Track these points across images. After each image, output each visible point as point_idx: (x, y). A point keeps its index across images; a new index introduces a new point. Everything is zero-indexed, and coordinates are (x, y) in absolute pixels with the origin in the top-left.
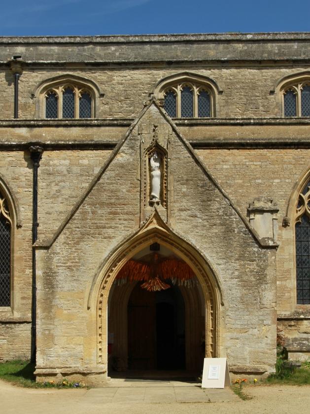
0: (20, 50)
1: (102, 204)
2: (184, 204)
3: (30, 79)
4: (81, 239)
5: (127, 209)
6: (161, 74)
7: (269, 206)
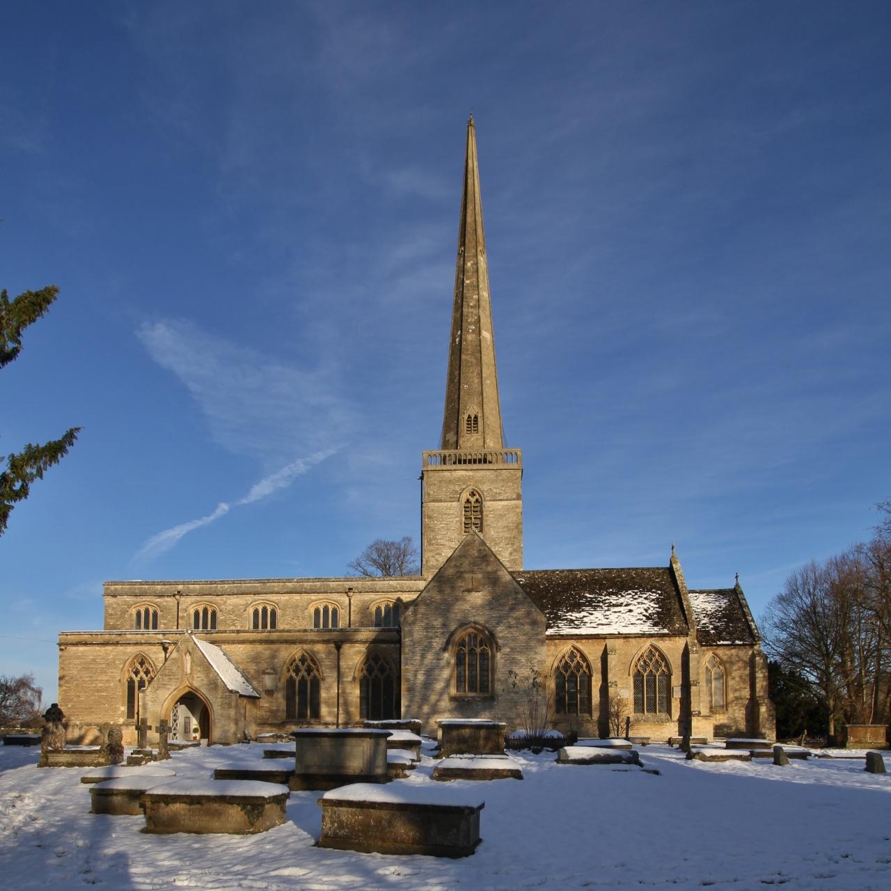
1: (166, 675)
2: (199, 675)
4: (157, 690)
5: (177, 677)
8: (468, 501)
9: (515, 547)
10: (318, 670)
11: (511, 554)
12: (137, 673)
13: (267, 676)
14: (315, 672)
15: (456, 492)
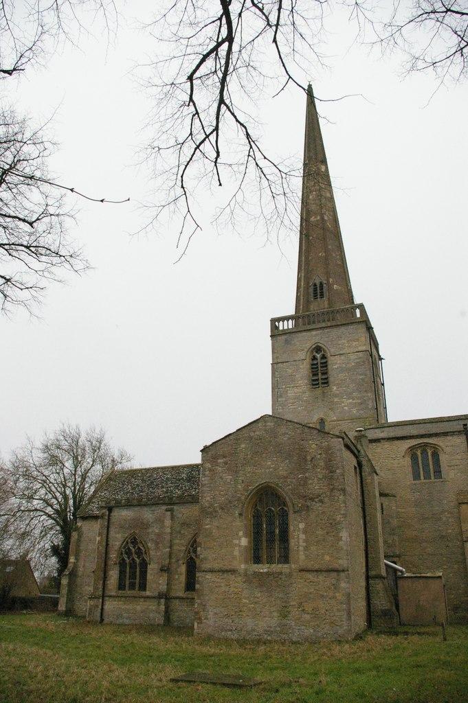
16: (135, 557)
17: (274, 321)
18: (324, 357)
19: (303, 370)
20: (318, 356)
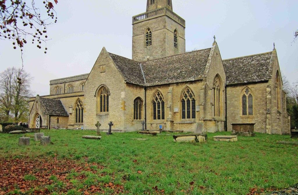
0: (65, 80)
3: (67, 84)
6: (81, 82)
7: (71, 107)
8: (147, 33)
9: (163, 49)
10: (194, 96)
11: (161, 52)
12: (78, 106)
13: (70, 108)
14: (193, 97)
15: (143, 30)
16: (80, 107)
17: (135, 19)
18: (151, 32)
19: (142, 38)
20: (149, 32)
